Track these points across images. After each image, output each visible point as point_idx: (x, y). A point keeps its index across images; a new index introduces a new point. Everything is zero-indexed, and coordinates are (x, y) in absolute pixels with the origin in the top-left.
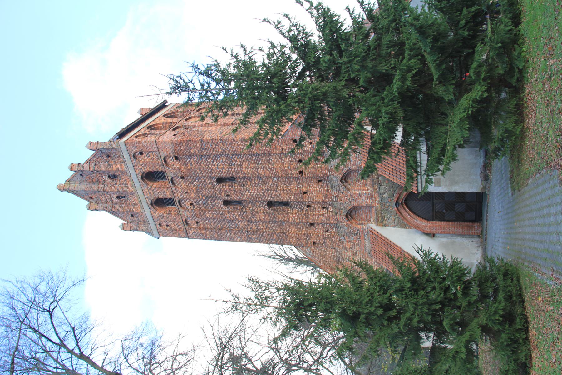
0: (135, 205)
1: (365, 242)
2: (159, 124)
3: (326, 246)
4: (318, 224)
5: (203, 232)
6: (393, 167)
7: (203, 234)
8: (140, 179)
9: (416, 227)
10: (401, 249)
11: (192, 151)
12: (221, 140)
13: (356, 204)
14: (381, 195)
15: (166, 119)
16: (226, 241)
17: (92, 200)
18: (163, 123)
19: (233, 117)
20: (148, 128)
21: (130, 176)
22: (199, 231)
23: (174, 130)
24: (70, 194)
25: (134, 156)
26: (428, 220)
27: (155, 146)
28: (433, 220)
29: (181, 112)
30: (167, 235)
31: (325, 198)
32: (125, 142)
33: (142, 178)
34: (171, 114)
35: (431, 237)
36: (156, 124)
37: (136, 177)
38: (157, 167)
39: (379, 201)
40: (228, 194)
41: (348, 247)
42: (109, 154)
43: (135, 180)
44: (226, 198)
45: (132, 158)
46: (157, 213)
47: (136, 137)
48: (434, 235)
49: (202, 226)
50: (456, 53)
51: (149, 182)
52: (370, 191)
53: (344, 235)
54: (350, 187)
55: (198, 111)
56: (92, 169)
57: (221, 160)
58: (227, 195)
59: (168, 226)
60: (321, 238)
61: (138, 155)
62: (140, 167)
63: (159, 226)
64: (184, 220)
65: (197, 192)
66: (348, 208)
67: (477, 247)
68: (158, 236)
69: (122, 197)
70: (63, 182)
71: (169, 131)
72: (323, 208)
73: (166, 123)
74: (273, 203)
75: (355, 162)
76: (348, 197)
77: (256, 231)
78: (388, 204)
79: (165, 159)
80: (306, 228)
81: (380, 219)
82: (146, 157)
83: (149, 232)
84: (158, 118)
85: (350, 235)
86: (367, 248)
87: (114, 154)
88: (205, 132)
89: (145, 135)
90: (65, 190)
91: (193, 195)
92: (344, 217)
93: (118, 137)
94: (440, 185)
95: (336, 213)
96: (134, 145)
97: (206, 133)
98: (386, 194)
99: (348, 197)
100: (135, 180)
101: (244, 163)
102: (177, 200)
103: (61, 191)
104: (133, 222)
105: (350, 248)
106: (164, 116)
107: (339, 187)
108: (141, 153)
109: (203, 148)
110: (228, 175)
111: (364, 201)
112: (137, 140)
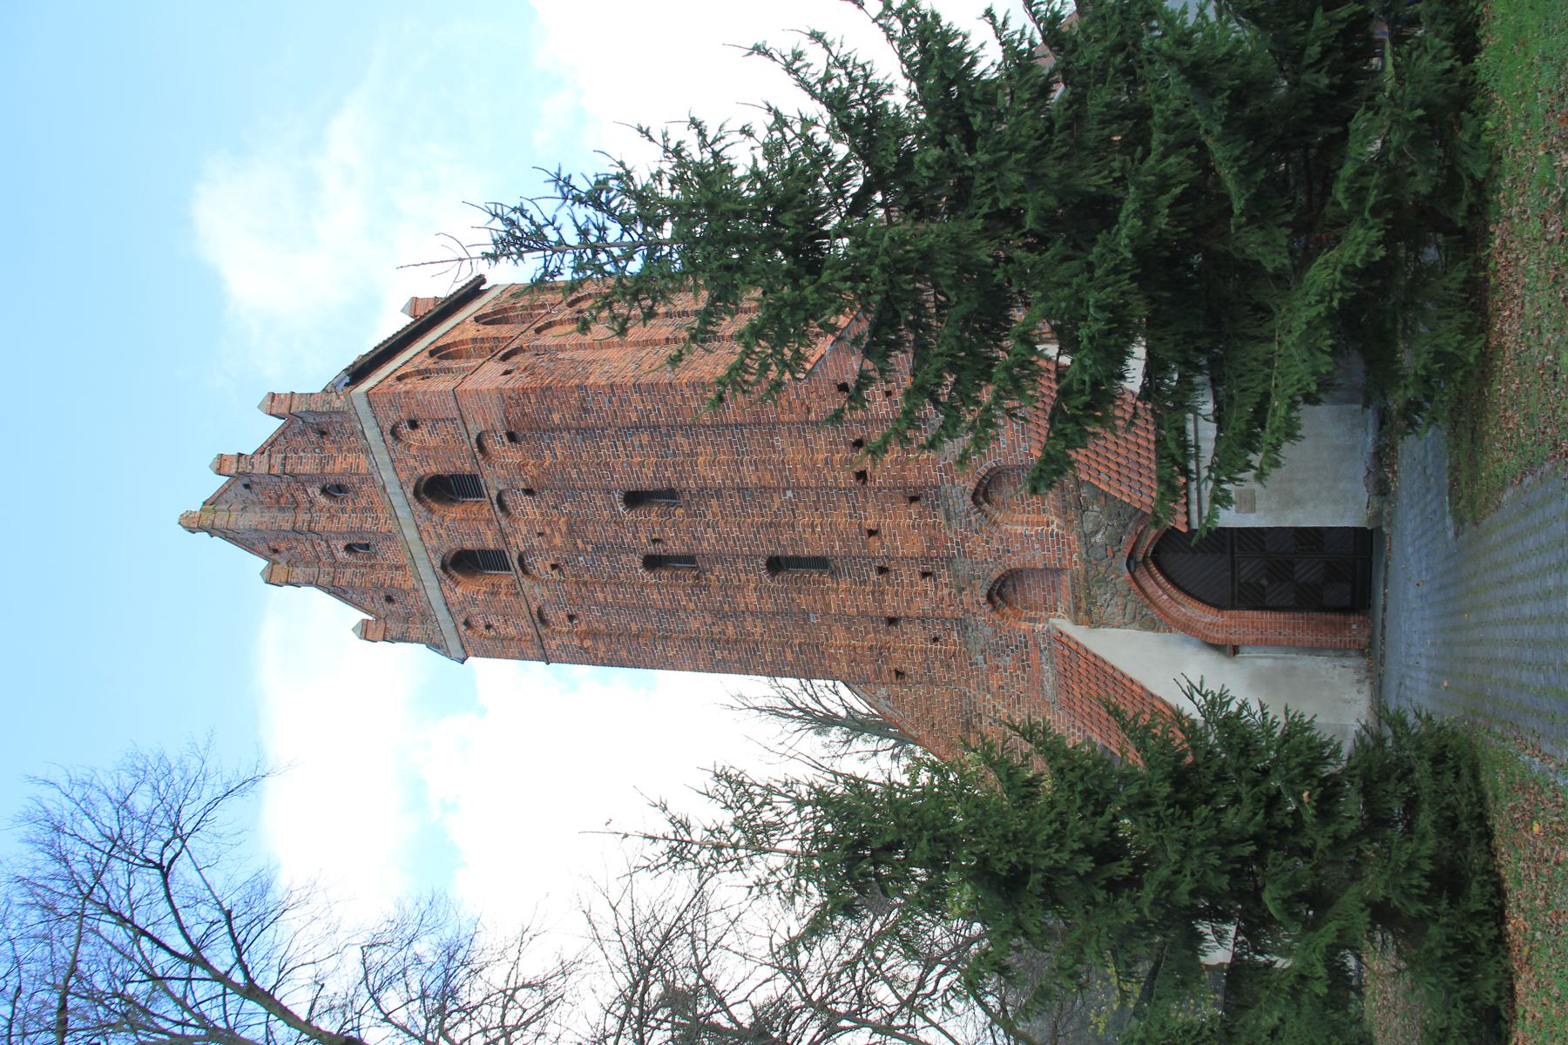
0: (397, 568)
1: (1040, 671)
2: (462, 342)
4: (909, 620)
5: (588, 643)
7: (586, 650)
8: (410, 496)
9: (1187, 628)
11: (556, 417)
12: (638, 387)
13: (1015, 563)
14: (1086, 537)
15: (481, 327)
16: (653, 668)
17: (276, 557)
18: (474, 340)
19: (669, 321)
20: (432, 353)
22: (576, 642)
23: (505, 358)
25: (394, 432)
26: (1219, 606)
27: (452, 404)
28: (1233, 608)
30: (487, 654)
31: (929, 549)
32: (367, 393)
33: (416, 493)
34: (495, 313)
36: (455, 344)
37: (398, 490)
38: (458, 464)
40: (655, 536)
41: (994, 683)
43: (398, 500)
44: (651, 549)
45: (389, 438)
46: (459, 590)
47: (400, 379)
48: (1235, 650)
49: (583, 627)
51: (436, 506)
54: (998, 516)
55: (571, 305)
58: (655, 541)
59: (488, 627)
60: (919, 658)
61: (405, 429)
62: (412, 462)
63: (463, 628)
64: (534, 609)
65: (570, 531)
66: (995, 575)
67: (1359, 681)
70: (197, 507)
71: (492, 363)
72: (925, 575)
74: (417, 537)
75: (1013, 447)
76: (995, 545)
77: (736, 641)
78: (1105, 562)
79: (479, 440)
80: (876, 631)
81: (1083, 604)
83: (437, 646)
85: (999, 651)
88: (591, 363)
89: (424, 374)
90: (201, 529)
91: (558, 541)
92: (983, 600)
93: (347, 380)
94: (1253, 510)
97: (595, 366)
98: (1099, 536)
99: (995, 545)
100: (398, 500)
101: (700, 449)
102: (515, 556)
104: (392, 617)
105: (1001, 687)
106: (477, 319)
107: (968, 515)
108: (414, 425)
109: (585, 410)
110: (657, 485)
112: (401, 387)
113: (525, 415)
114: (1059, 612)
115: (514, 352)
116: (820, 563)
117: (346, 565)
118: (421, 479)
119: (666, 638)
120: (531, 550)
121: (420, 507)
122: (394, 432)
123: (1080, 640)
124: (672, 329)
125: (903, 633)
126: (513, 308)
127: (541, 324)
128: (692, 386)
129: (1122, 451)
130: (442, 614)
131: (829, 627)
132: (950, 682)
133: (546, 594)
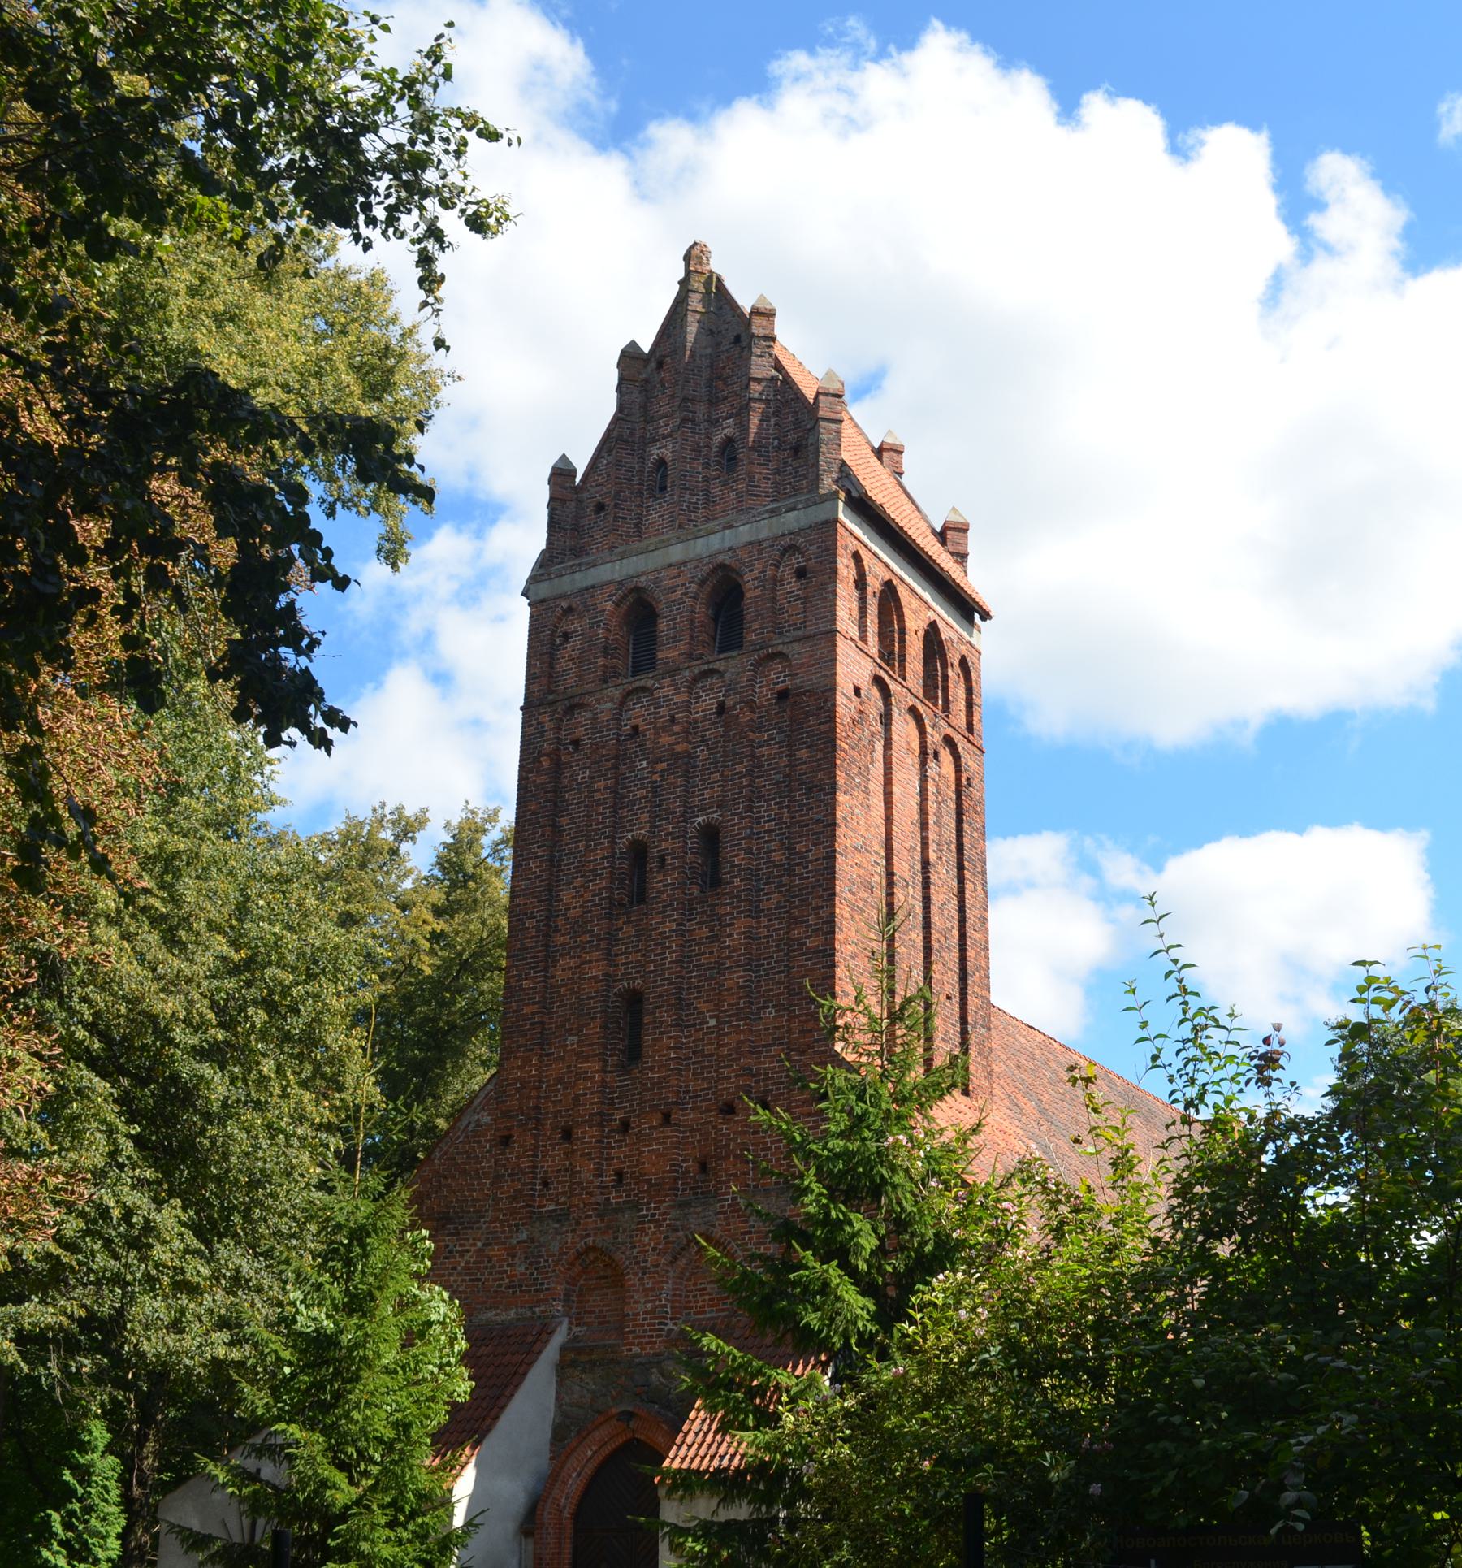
0: (637, 525)
1: (507, 1308)
3: (498, 1178)
4: (570, 1154)
5: (545, 762)
7: (537, 760)
8: (721, 557)
9: (552, 1478)
11: (803, 754)
13: (632, 1280)
15: (921, 633)
17: (653, 365)
18: (902, 631)
21: (730, 527)
23: (878, 681)
24: (677, 287)
25: (791, 549)
30: (533, 619)
33: (722, 566)
35: (522, 1525)
36: (899, 608)
37: (727, 545)
38: (755, 626)
39: (637, 1356)
41: (495, 1251)
44: (654, 853)
45: (787, 541)
46: (609, 606)
47: (856, 556)
49: (565, 758)
50: (43, 828)
51: (707, 588)
53: (532, 1240)
55: (949, 741)
57: (772, 846)
58: (662, 859)
59: (566, 636)
60: (525, 1163)
61: (797, 561)
63: (565, 605)
65: (676, 756)
66: (618, 1256)
69: (664, 476)
70: (716, 265)
72: (620, 1174)
73: (902, 641)
74: (670, 556)
77: (547, 946)
79: (780, 654)
80: (556, 1114)
81: (583, 1358)
82: (788, 588)
83: (546, 564)
84: (921, 607)
86: (490, 1314)
88: (867, 792)
89: (861, 583)
91: (665, 739)
93: (855, 494)
95: (601, 1216)
97: (861, 796)
100: (715, 542)
101: (764, 922)
102: (650, 683)
103: (687, 258)
106: (933, 625)
108: (801, 573)
109: (809, 790)
111: (640, 1308)
113: (807, 715)
114: (576, 1329)
116: (634, 1053)
117: (643, 459)
119: (551, 861)
121: (706, 569)
122: (791, 549)
125: (553, 1146)
130: (583, 579)
131: (562, 1059)
132: (497, 1199)
133: (604, 717)
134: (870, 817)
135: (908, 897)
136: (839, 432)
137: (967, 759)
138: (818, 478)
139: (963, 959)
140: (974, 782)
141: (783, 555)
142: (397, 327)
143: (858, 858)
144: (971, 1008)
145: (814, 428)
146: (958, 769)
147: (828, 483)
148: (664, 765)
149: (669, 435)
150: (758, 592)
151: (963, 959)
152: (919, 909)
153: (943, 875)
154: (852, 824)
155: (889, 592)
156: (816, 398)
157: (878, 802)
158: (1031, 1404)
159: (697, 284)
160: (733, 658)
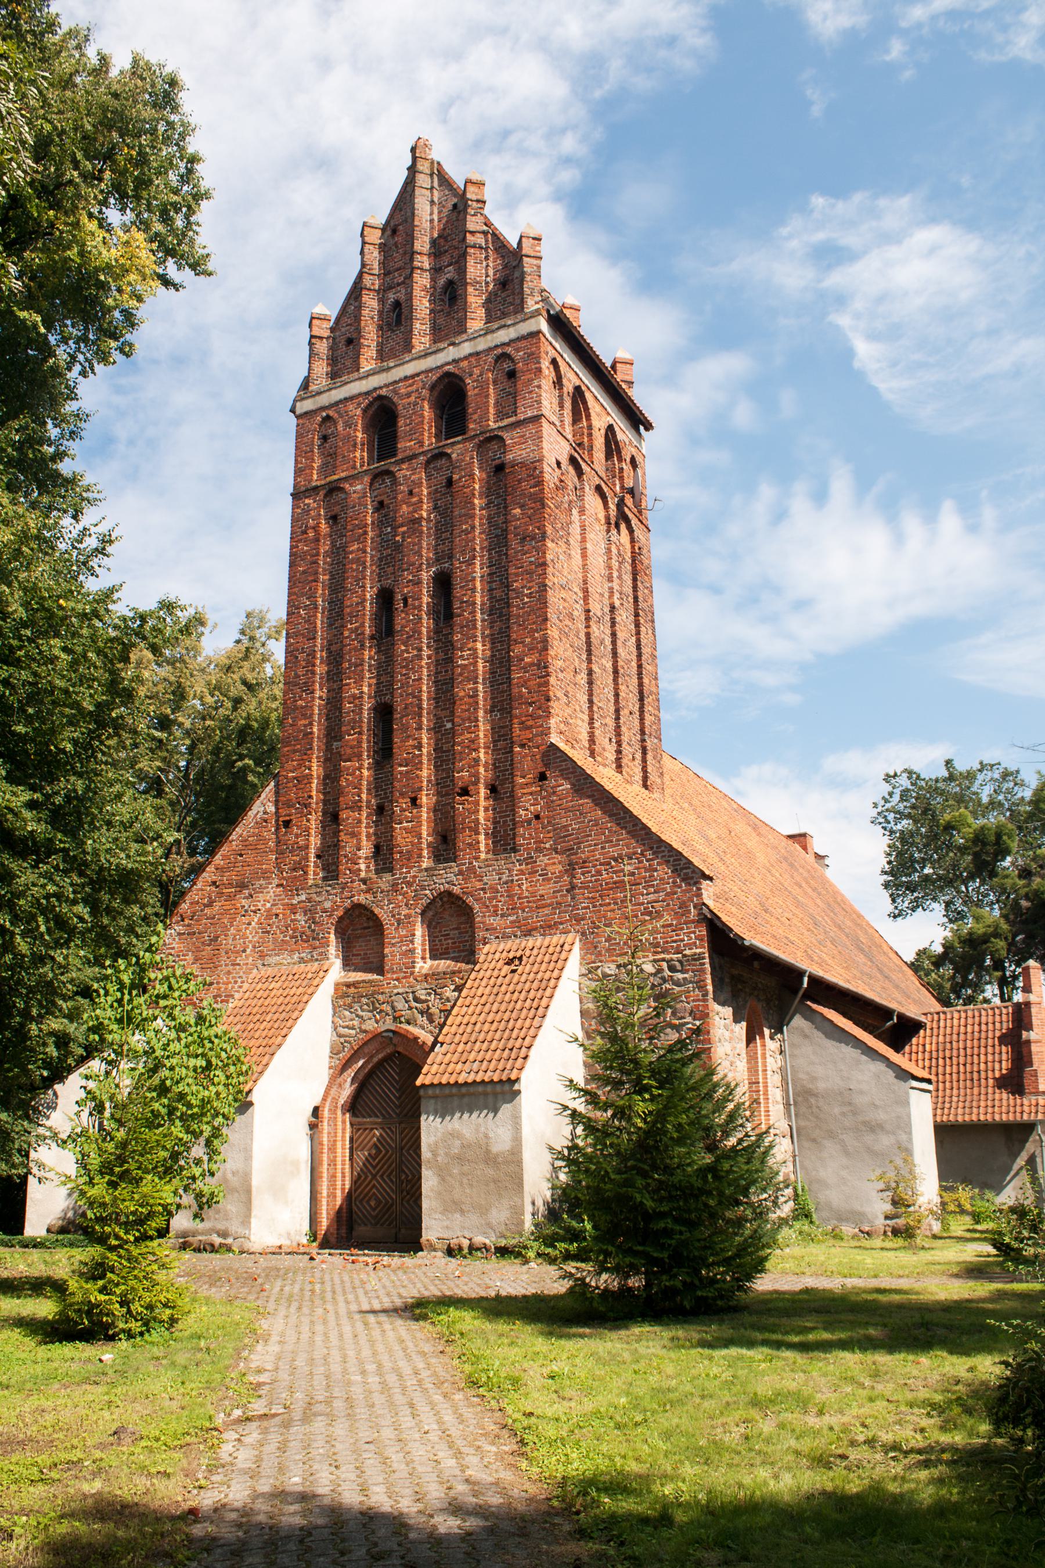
2: (588, 417)
6: (479, 1025)
7: (305, 532)
10: (280, 1046)
15: (603, 432)
16: (290, 594)
18: (590, 427)
19: (607, 610)
23: (573, 461)
24: (406, 173)
27: (530, 414)
29: (621, 470)
32: (539, 332)
34: (617, 443)
36: (587, 409)
37: (450, 359)
38: (475, 417)
42: (509, 287)
45: (500, 351)
46: (359, 412)
47: (554, 362)
52: (421, 964)
53: (309, 900)
56: (470, 238)
58: (405, 600)
62: (477, 371)
66: (377, 911)
67: (289, 1234)
68: (298, 411)
69: (399, 316)
70: (435, 155)
71: (568, 448)
73: (590, 435)
81: (352, 990)
84: (603, 413)
85: (309, 912)
87: (510, 299)
88: (567, 543)
89: (558, 382)
90: (415, 159)
96: (534, 357)
97: (564, 546)
103: (413, 150)
109: (524, 539)
110: (456, 605)
112: (545, 364)
113: (519, 481)
115: (580, 473)
118: (462, 380)
120: (395, 482)
123: (321, 987)
124: (599, 614)
126: (620, 459)
127: (605, 489)
128: (545, 641)
129: (486, 1027)
134: (577, 555)
135: (600, 632)
136: (539, 267)
137: (638, 533)
138: (522, 302)
139: (641, 685)
140: (644, 551)
141: (496, 361)
142: (71, 1282)
143: (563, 594)
144: (647, 723)
145: (521, 260)
146: (633, 541)
147: (532, 304)
148: (405, 529)
149: (403, 283)
150: (476, 391)
151: (641, 685)
152: (608, 641)
153: (624, 617)
154: (558, 566)
155: (578, 393)
156: (520, 243)
157: (576, 553)
158: (949, 847)
159: (423, 166)
160: (458, 442)
